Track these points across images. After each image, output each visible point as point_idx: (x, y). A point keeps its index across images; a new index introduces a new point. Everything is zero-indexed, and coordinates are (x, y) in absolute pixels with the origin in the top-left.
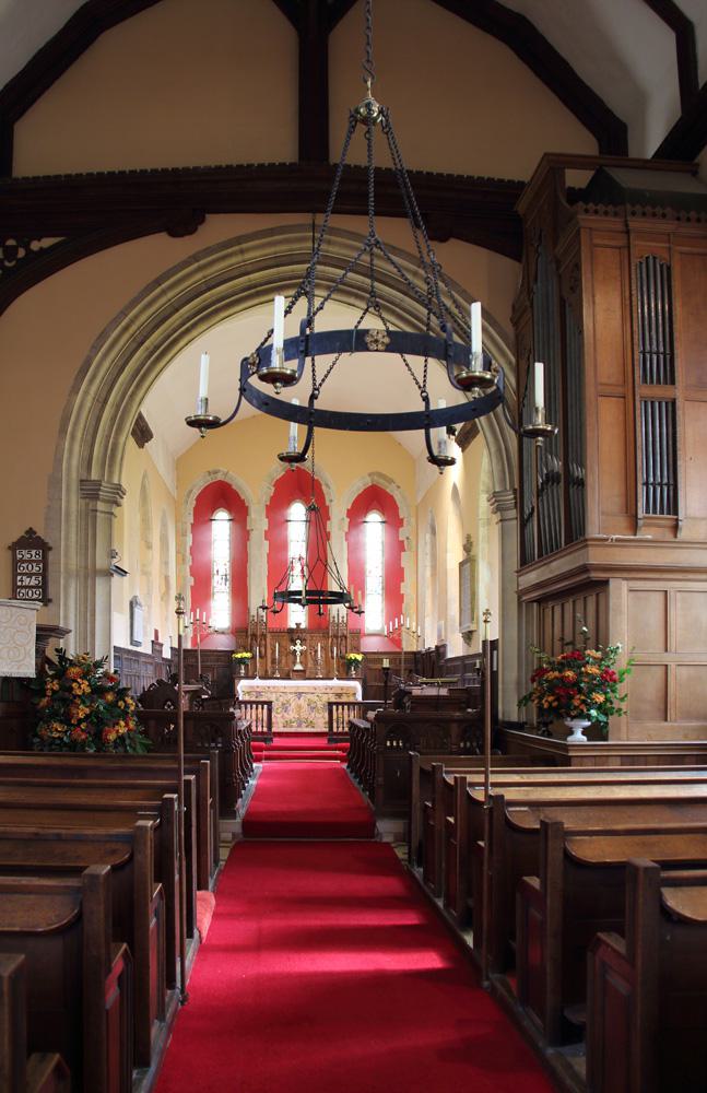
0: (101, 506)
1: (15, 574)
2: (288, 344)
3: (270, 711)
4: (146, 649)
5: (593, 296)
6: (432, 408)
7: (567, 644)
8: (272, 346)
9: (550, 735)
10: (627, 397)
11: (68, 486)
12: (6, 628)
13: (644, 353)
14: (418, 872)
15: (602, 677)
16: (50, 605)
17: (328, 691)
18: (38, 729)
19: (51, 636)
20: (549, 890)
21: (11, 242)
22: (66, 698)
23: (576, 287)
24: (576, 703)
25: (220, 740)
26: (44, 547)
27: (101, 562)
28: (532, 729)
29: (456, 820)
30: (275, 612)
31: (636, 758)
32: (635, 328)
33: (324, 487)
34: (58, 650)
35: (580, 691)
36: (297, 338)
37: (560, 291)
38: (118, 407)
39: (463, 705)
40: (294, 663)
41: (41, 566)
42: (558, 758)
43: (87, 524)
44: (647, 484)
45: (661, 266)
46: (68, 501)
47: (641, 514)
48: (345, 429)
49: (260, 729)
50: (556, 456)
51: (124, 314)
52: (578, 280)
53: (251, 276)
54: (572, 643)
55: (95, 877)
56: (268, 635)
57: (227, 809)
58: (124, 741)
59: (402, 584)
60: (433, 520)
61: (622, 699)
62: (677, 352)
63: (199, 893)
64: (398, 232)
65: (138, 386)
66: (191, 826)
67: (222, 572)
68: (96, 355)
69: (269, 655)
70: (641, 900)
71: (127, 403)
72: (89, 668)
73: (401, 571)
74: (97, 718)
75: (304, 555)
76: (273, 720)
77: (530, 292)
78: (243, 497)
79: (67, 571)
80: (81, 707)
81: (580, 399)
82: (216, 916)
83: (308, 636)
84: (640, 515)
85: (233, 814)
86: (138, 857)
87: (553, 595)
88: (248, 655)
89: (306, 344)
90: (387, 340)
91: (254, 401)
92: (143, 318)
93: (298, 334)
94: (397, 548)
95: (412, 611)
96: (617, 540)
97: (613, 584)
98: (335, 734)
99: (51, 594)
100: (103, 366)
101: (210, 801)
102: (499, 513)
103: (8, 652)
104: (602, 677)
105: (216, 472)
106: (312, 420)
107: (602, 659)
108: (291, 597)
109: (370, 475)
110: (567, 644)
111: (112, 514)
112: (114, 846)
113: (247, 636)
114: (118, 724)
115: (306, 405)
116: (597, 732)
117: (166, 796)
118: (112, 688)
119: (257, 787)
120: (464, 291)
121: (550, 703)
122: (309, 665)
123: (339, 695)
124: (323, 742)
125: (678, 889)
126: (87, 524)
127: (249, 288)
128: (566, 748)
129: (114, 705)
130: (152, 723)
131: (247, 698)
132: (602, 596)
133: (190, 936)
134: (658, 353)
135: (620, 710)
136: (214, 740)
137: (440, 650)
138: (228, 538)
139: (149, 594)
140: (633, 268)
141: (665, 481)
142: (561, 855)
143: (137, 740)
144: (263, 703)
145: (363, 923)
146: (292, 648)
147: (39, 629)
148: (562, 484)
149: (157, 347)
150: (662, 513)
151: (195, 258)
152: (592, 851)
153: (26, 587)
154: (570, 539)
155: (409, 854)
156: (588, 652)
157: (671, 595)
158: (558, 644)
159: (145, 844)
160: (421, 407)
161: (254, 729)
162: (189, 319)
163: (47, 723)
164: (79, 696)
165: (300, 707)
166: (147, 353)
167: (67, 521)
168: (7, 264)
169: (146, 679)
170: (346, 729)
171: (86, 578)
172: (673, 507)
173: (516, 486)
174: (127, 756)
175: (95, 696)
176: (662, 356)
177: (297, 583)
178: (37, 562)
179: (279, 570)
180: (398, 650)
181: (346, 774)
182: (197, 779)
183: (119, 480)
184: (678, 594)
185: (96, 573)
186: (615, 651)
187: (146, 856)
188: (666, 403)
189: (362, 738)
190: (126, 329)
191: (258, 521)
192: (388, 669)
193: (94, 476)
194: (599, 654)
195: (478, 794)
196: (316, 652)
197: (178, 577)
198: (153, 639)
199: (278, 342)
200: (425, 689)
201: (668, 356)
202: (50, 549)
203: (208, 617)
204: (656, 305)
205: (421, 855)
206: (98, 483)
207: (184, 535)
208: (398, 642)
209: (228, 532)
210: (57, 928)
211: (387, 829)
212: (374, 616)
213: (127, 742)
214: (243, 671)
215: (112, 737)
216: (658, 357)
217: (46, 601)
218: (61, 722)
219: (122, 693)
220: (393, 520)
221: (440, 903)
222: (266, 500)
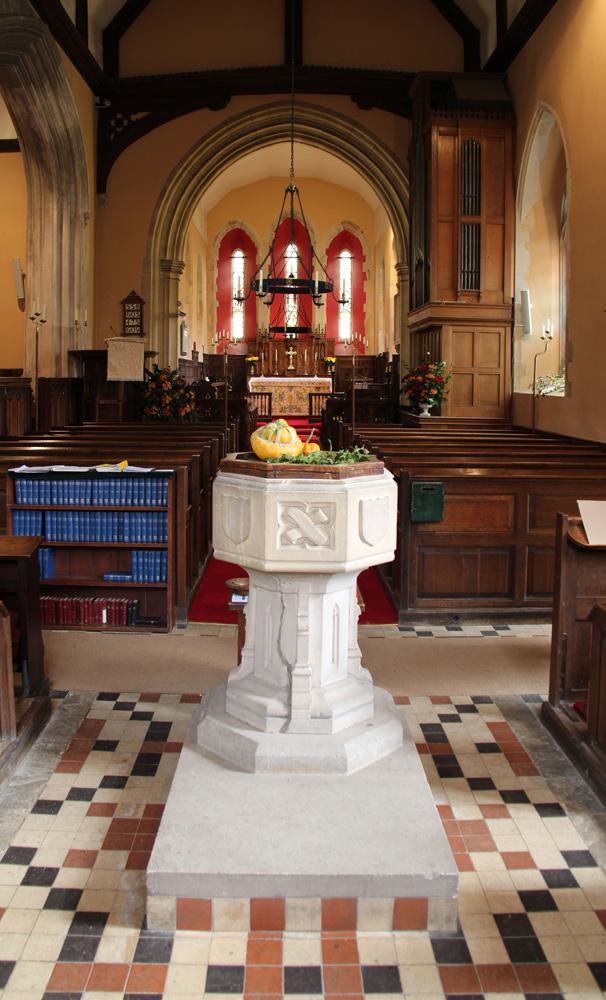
1: (125, 318)
3: (270, 400)
4: (189, 357)
21: (119, 116)
22: (159, 392)
24: (422, 394)
26: (140, 301)
27: (172, 310)
35: (425, 388)
38: (181, 214)
40: (288, 364)
51: (185, 159)
64: (343, 103)
65: (193, 201)
73: (364, 294)
76: (273, 407)
78: (253, 240)
79: (154, 316)
88: (256, 358)
92: (196, 160)
98: (315, 416)
100: (172, 192)
105: (234, 222)
109: (343, 223)
116: (434, 411)
123: (318, 388)
128: (418, 419)
129: (183, 396)
131: (255, 391)
138: (242, 270)
144: (267, 394)
149: (203, 177)
151: (225, 123)
161: (259, 413)
163: (150, 407)
165: (291, 397)
167: (154, 286)
168: (118, 130)
171: (164, 319)
172: (478, 286)
190: (186, 168)
193: (168, 257)
196: (303, 356)
206: (171, 261)
209: (243, 266)
215: (183, 414)
220: (359, 258)
222: (269, 242)
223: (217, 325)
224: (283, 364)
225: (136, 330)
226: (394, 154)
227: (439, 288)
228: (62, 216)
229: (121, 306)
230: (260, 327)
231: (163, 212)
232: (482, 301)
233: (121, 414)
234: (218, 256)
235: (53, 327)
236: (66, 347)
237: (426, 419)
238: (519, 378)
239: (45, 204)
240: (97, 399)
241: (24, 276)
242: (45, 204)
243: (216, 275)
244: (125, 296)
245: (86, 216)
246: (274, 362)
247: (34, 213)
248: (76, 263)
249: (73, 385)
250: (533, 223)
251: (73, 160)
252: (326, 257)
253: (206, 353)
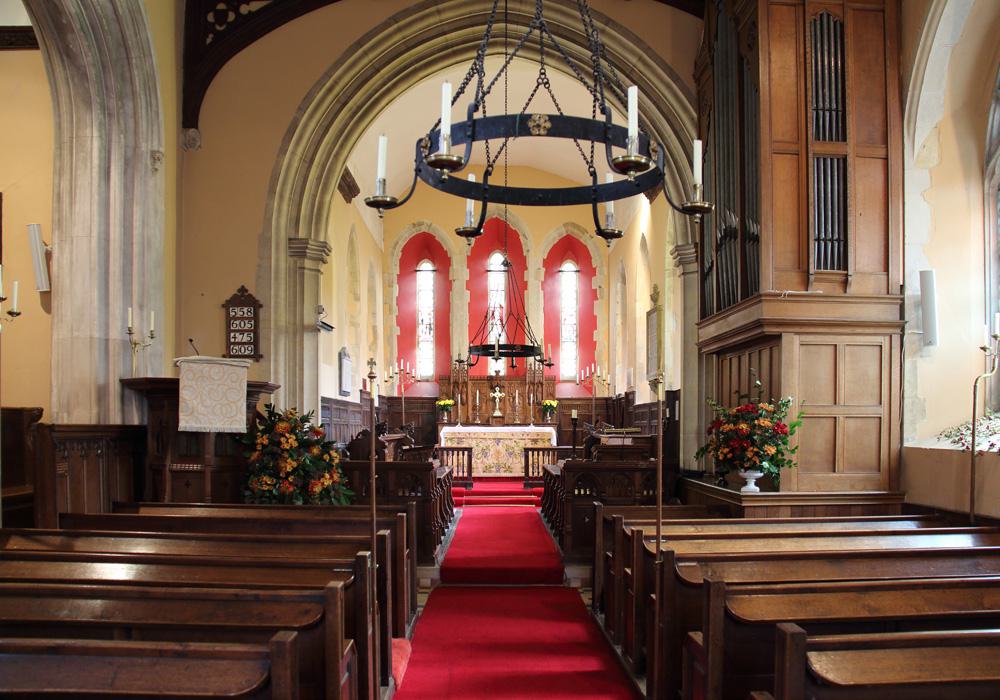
0: (308, 263)
1: (229, 331)
2: (455, 129)
5: (770, 54)
6: (599, 182)
7: (742, 397)
8: (440, 130)
9: (726, 485)
10: (800, 155)
11: (277, 245)
12: (219, 385)
13: (817, 110)
14: (600, 618)
15: (774, 430)
16: (261, 360)
18: (250, 482)
19: (260, 392)
20: (710, 649)
21: (221, 6)
22: (275, 452)
23: (753, 46)
25: (420, 489)
26: (255, 305)
27: (308, 319)
28: (711, 478)
29: (632, 571)
30: (472, 365)
31: (806, 509)
32: (809, 85)
33: (521, 238)
34: (268, 406)
35: (753, 443)
36: (464, 123)
37: (739, 47)
39: (646, 455)
40: (494, 410)
41: (252, 335)
42: (732, 509)
43: (295, 282)
44: (818, 240)
45: (835, 23)
46: (277, 260)
47: (812, 269)
48: (518, 204)
49: (461, 474)
50: (734, 212)
51: (328, 75)
52: (755, 39)
53: (448, 36)
54: (747, 396)
55: (280, 644)
57: (425, 556)
58: (330, 492)
59: (595, 332)
60: (623, 269)
61: (793, 451)
62: (849, 108)
63: (395, 641)
65: (342, 146)
66: (386, 579)
67: (426, 321)
68: (303, 115)
69: (470, 403)
70: (788, 665)
71: (332, 163)
72: (296, 423)
73: (594, 318)
74: (304, 470)
75: (504, 304)
77: (711, 48)
80: (289, 460)
81: (756, 155)
82: (412, 663)
83: (506, 384)
84: (812, 271)
85: (431, 561)
86: (329, 617)
87: (732, 347)
88: (451, 402)
89: (470, 130)
90: (548, 125)
91: (431, 181)
92: (346, 79)
93: (465, 119)
94: (590, 297)
95: (604, 358)
96: (789, 295)
97: (785, 338)
98: (536, 478)
99: (262, 350)
100: (309, 127)
101: (406, 552)
102: (681, 267)
103: (221, 408)
104: (774, 430)
105: (420, 224)
106: (487, 196)
107: (774, 412)
108: (486, 350)
109: (565, 225)
110: (742, 397)
111: (319, 271)
112: (308, 606)
113: (449, 384)
114: (323, 476)
115: (481, 181)
116: (768, 483)
117: (360, 553)
118: (317, 442)
119: (457, 533)
120: (649, 48)
121: (725, 455)
123: (535, 441)
124: (520, 486)
125: (821, 653)
126: (295, 282)
127: (446, 47)
128: (739, 498)
129: (320, 458)
130: (357, 474)
131: (449, 445)
132: (775, 350)
133: (385, 683)
134: (830, 110)
135: (790, 461)
136: (413, 489)
137: (629, 396)
138: (432, 288)
139: (357, 345)
140: (808, 25)
141: (836, 236)
142: (722, 613)
143: (341, 491)
144: (464, 449)
145: (547, 669)
146: (492, 395)
147: (249, 385)
148: (739, 239)
149: (360, 108)
150: (832, 268)
152: (756, 609)
153: (239, 344)
154: (745, 295)
155: (593, 599)
156: (761, 405)
157: (840, 349)
158: (735, 397)
159: (336, 603)
160: (589, 182)
161: (455, 474)
162: (390, 79)
163: (258, 475)
164: (287, 450)
165: (498, 452)
166: (350, 113)
167: (277, 278)
168: (218, 28)
169: (355, 426)
170: (541, 474)
171: (295, 334)
173: (698, 240)
174: (331, 508)
175: (302, 450)
176: (834, 113)
177: (496, 335)
178: (249, 319)
179: (480, 321)
180: (590, 396)
181: (540, 518)
182: (394, 534)
183: (325, 237)
184: (847, 348)
185: (304, 328)
186: (786, 404)
187: (336, 616)
188: (838, 160)
189: (554, 483)
190: (330, 90)
191: (460, 272)
192: (576, 419)
193: (302, 234)
194: (771, 407)
195: (651, 547)
196: (514, 398)
197: (384, 322)
198: (361, 388)
199: (445, 130)
200: (611, 438)
201: (840, 113)
202: (261, 306)
203: (413, 366)
204: (830, 61)
205: (603, 602)
206: (305, 241)
207: (391, 286)
208: (589, 388)
210: (250, 692)
211: (574, 574)
212: (568, 363)
213: (332, 493)
215: (318, 489)
216: (824, 114)
217: (257, 356)
218: (270, 476)
219: (327, 447)
220: (587, 270)
221: (619, 650)
224: (487, 409)
225: (248, 350)
226: (671, 69)
227: (776, 269)
228: (109, 152)
229: (224, 310)
231: (296, 152)
232: (852, 290)
233: (208, 488)
234: (398, 267)
235: (91, 338)
236: (118, 371)
237: (754, 497)
238: (913, 423)
239: (78, 128)
240: (168, 462)
241: (48, 255)
242: (78, 128)
243: (396, 293)
244: (228, 296)
245: (155, 157)
247: (65, 147)
248: (137, 232)
249: (124, 438)
250: (935, 155)
251: (128, 58)
252: (544, 269)
253: (383, 394)
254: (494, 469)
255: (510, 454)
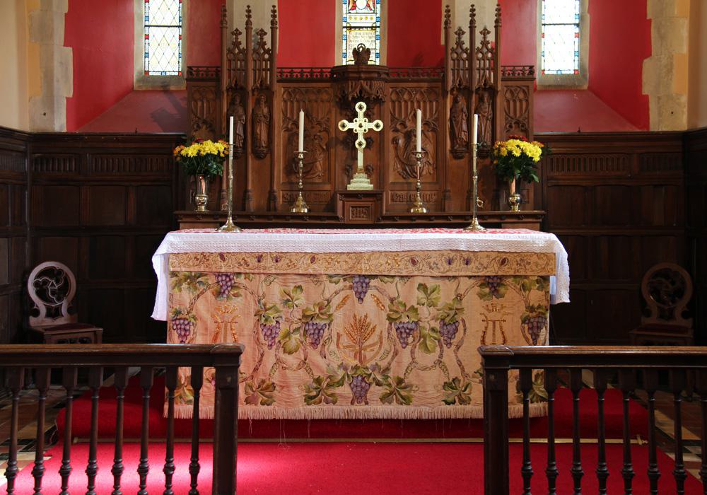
17: (458, 268)
40: (350, 171)
56: (279, 89)
113: (218, 93)
122: (392, 178)
165: (361, 328)
196: (410, 136)
214: (203, 198)
223: (70, 18)
224: (328, 169)
230: (238, 22)
246: (291, 161)
254: (345, 390)
255: (405, 333)
